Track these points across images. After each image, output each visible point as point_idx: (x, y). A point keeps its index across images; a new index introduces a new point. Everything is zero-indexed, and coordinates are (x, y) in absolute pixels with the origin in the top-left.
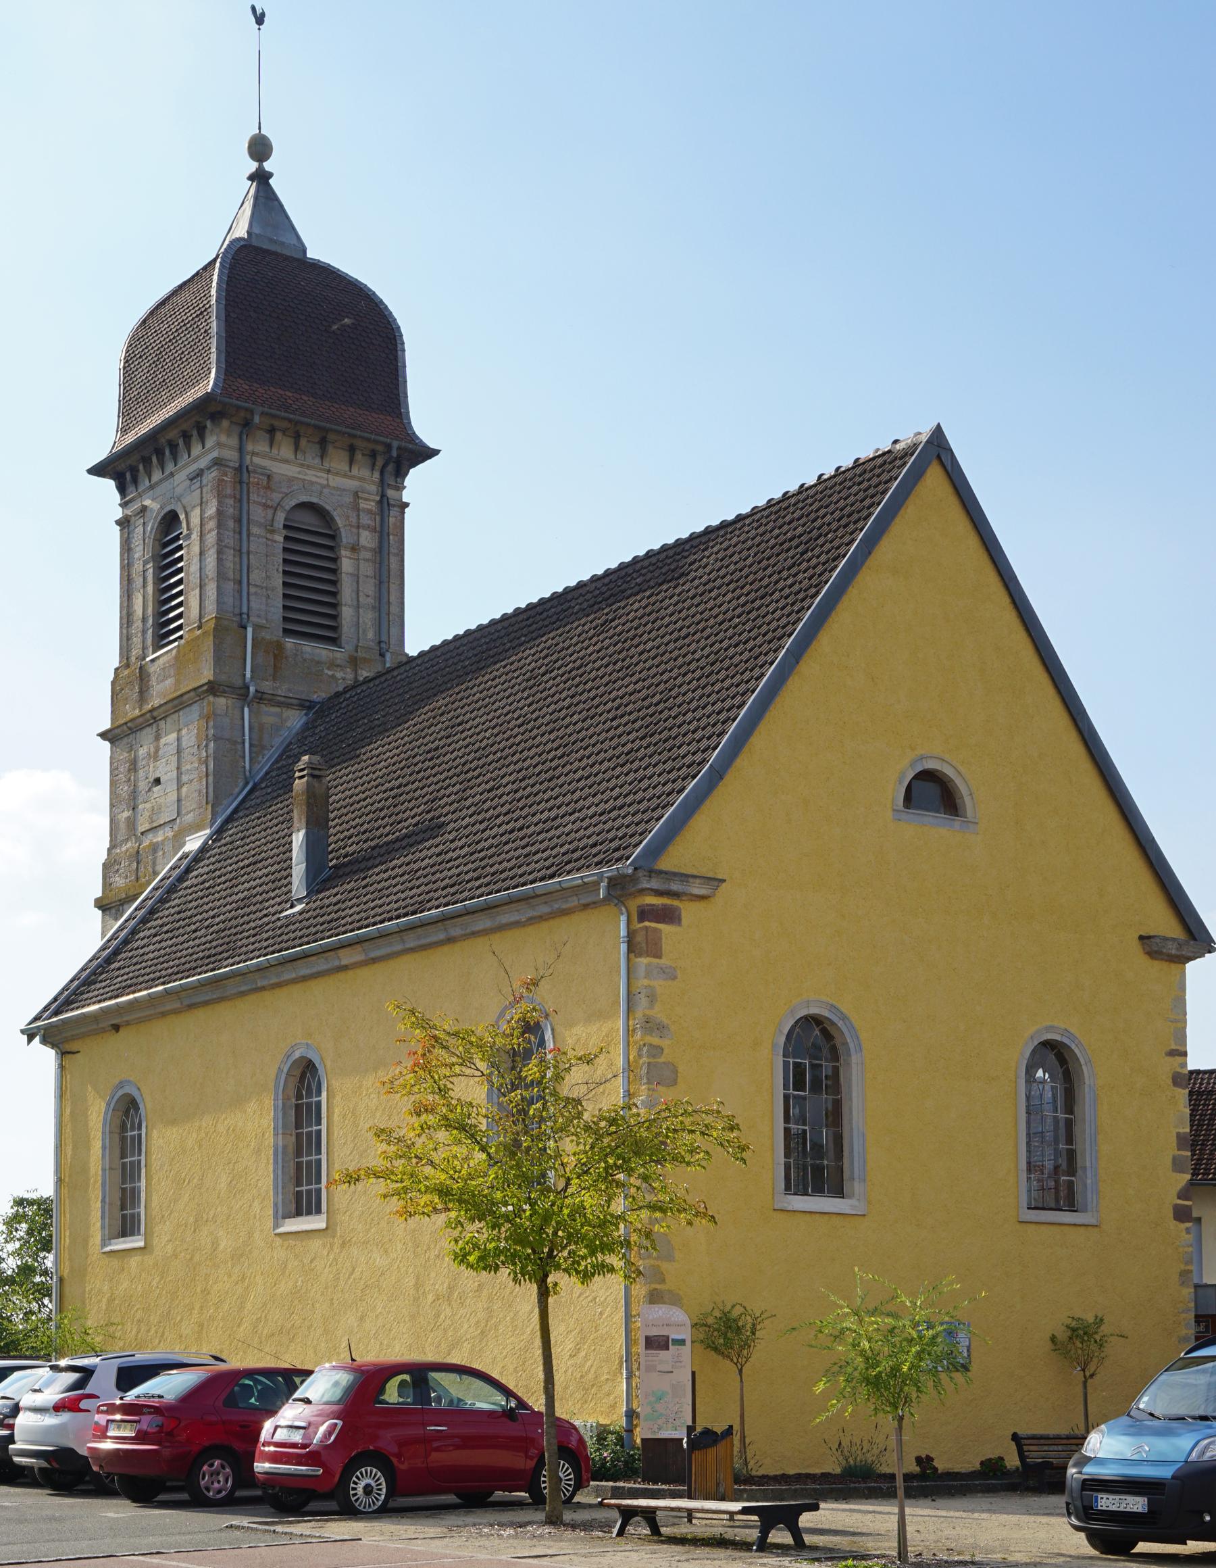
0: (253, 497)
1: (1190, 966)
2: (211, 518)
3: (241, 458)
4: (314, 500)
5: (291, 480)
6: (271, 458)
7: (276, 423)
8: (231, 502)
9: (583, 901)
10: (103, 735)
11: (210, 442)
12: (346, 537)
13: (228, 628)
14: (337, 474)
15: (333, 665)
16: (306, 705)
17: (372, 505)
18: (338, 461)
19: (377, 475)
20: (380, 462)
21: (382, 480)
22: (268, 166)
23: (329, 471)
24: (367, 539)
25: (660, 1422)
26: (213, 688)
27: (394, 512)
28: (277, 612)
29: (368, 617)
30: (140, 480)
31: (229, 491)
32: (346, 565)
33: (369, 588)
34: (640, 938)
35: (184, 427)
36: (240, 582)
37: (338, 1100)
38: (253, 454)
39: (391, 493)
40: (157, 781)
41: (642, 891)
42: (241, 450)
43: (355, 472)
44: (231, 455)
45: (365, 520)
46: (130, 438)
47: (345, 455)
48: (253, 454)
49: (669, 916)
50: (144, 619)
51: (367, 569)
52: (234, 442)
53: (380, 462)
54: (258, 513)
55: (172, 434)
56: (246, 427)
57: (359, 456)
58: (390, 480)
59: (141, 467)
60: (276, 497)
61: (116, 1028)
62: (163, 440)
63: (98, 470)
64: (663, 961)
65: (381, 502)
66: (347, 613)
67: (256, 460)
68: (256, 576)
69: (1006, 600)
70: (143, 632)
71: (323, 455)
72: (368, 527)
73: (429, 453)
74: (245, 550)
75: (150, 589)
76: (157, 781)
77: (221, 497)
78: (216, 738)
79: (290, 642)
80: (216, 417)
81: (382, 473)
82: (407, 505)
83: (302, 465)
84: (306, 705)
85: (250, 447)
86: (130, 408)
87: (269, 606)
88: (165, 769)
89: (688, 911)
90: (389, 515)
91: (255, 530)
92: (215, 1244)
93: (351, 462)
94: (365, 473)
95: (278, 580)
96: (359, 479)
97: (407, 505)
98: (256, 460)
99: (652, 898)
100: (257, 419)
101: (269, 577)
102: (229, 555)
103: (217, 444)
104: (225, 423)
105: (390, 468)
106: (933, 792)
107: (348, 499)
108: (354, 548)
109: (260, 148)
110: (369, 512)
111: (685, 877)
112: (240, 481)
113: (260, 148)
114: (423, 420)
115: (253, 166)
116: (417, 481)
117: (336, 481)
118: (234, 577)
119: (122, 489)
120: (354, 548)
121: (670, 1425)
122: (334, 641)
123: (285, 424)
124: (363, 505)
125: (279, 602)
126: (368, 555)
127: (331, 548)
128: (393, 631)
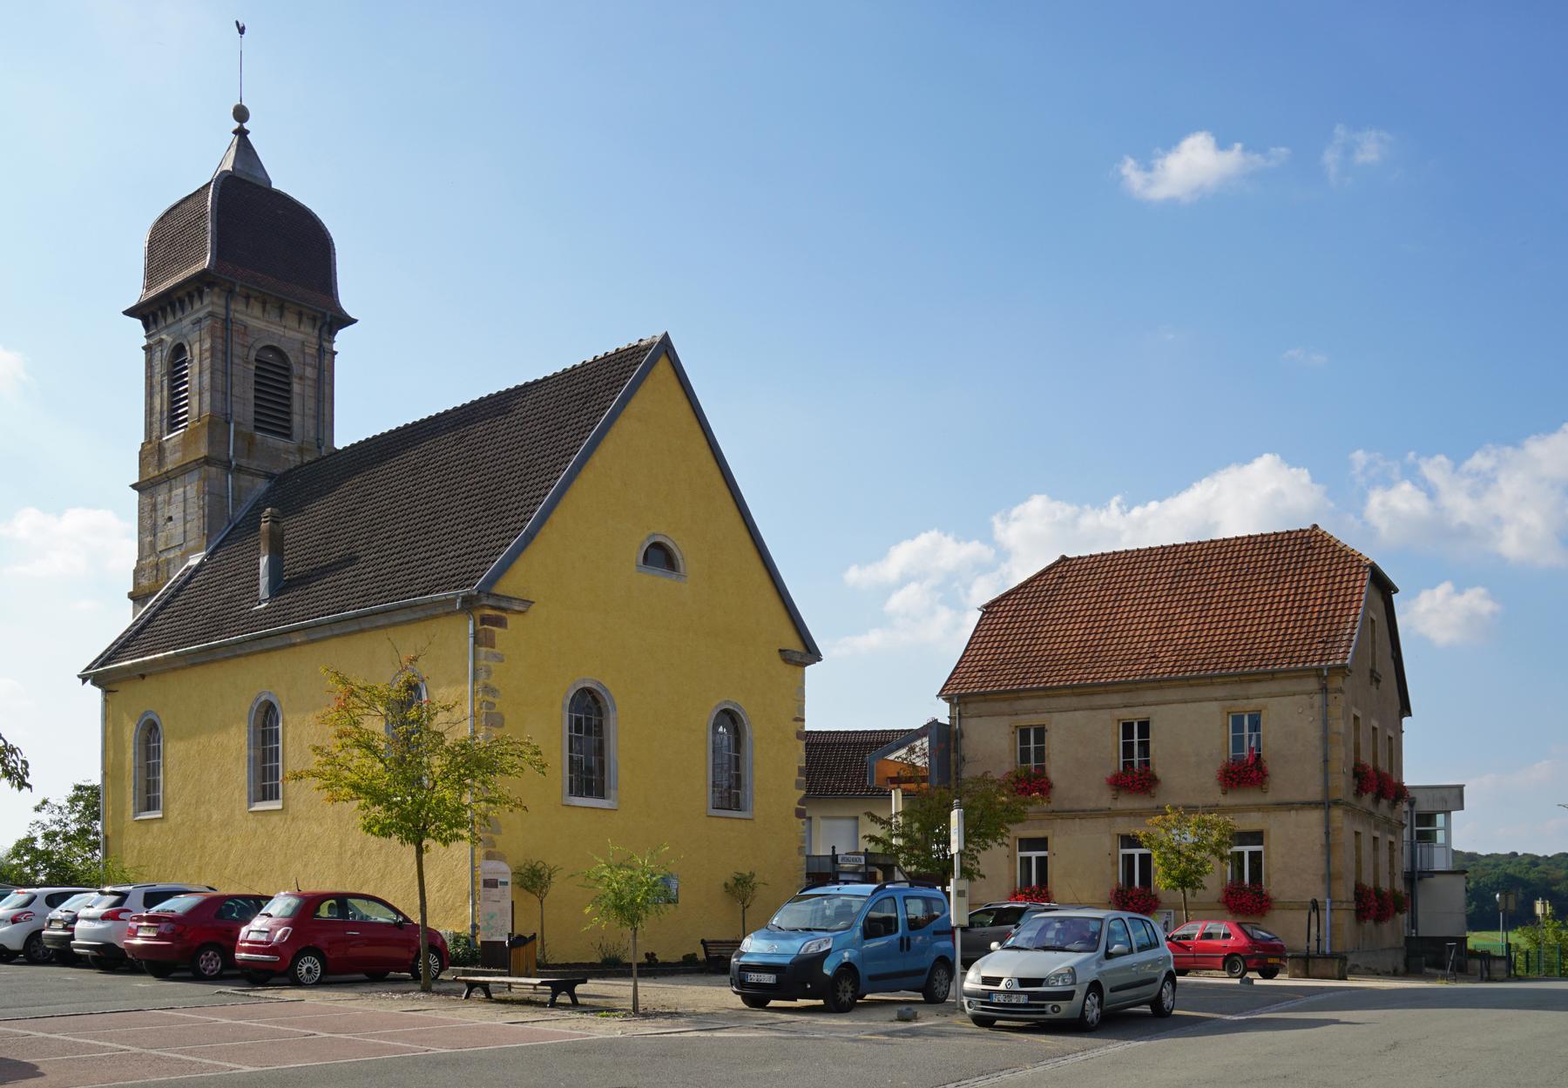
1: (807, 669)
5: (260, 330)
9: (444, 610)
10: (134, 486)
11: (206, 301)
12: (296, 369)
13: (218, 423)
15: (287, 451)
16: (269, 476)
17: (313, 351)
18: (291, 320)
20: (319, 324)
22: (246, 126)
26: (207, 461)
27: (328, 356)
29: (310, 423)
31: (219, 334)
32: (296, 388)
33: (311, 403)
34: (481, 635)
37: (290, 728)
41: (483, 606)
42: (227, 308)
44: (221, 311)
45: (309, 360)
46: (152, 293)
49: (500, 622)
50: (162, 413)
51: (310, 392)
52: (222, 302)
53: (319, 324)
54: (238, 350)
55: (181, 293)
56: (230, 294)
57: (305, 319)
58: (325, 336)
60: (251, 340)
61: (143, 677)
64: (496, 650)
66: (296, 419)
68: (236, 390)
69: (704, 442)
75: (165, 393)
76: (170, 519)
77: (213, 337)
78: (210, 493)
79: (259, 435)
80: (210, 285)
84: (269, 476)
85: (233, 306)
87: (245, 410)
88: (176, 512)
89: (512, 620)
90: (324, 359)
92: (210, 816)
93: (300, 322)
94: (309, 330)
95: (251, 394)
99: (489, 611)
102: (219, 375)
104: (216, 289)
106: (660, 556)
109: (241, 114)
111: (510, 599)
112: (226, 328)
113: (241, 114)
114: (348, 301)
115: (236, 125)
116: (342, 338)
117: (290, 334)
118: (222, 390)
119: (146, 326)
122: (289, 436)
125: (252, 409)
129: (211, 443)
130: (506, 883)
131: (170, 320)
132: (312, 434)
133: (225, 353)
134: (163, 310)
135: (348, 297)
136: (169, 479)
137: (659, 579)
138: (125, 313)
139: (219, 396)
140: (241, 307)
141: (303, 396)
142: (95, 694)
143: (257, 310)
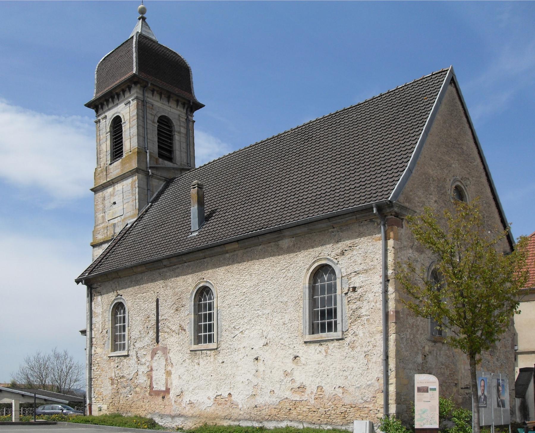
0: (148, 111)
2: (134, 116)
3: (144, 98)
4: (166, 115)
5: (159, 107)
6: (153, 100)
7: (155, 88)
8: (141, 111)
13: (141, 152)
14: (173, 108)
17: (184, 120)
19: (185, 111)
20: (186, 106)
21: (187, 113)
23: (170, 107)
24: (183, 130)
25: (424, 422)
27: (191, 123)
28: (156, 149)
29: (184, 155)
30: (104, 108)
31: (140, 107)
33: (184, 145)
35: (123, 87)
36: (145, 138)
38: (148, 97)
39: (190, 117)
40: (115, 203)
42: (143, 95)
43: (178, 108)
45: (182, 124)
46: (100, 94)
47: (175, 103)
48: (148, 97)
51: (183, 140)
52: (141, 92)
53: (186, 106)
54: (149, 116)
55: (117, 91)
56: (144, 88)
57: (180, 104)
58: (189, 113)
59: (105, 103)
60: (155, 112)
62: (114, 93)
63: (89, 105)
65: (186, 119)
67: (148, 99)
68: (149, 136)
70: (106, 156)
71: (168, 102)
72: (183, 126)
73: (201, 106)
74: (145, 127)
76: (115, 203)
80: (136, 83)
81: (187, 111)
82: (194, 122)
83: (163, 104)
85: (146, 95)
86: (99, 87)
87: (153, 147)
90: (189, 124)
91: (148, 121)
94: (182, 110)
96: (180, 111)
97: (194, 122)
98: (148, 99)
100: (149, 85)
101: (153, 137)
102: (141, 128)
103: (135, 92)
104: (139, 86)
105: (189, 109)
107: (177, 117)
108: (179, 132)
110: (183, 122)
112: (143, 107)
114: (199, 95)
116: (197, 115)
117: (174, 112)
118: (142, 135)
119: (97, 112)
120: (179, 132)
121: (429, 423)
123: (157, 89)
124: (181, 119)
126: (183, 135)
127: (170, 135)
128: (192, 161)
129: (139, 162)
130: (435, 389)
131: (110, 106)
132: (185, 161)
133: (144, 118)
134: (113, 98)
135: (199, 92)
136: (113, 183)
137: (256, 356)
138: (85, 105)
139: (141, 138)
140: (150, 95)
141: (180, 142)
142: (83, 288)
143: (157, 98)
